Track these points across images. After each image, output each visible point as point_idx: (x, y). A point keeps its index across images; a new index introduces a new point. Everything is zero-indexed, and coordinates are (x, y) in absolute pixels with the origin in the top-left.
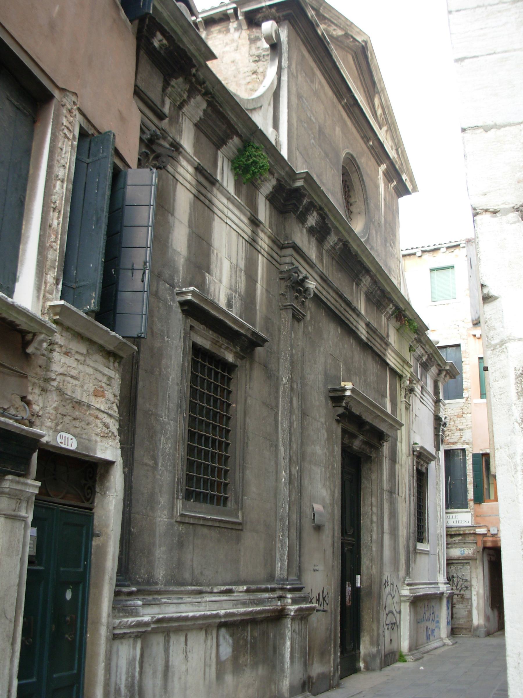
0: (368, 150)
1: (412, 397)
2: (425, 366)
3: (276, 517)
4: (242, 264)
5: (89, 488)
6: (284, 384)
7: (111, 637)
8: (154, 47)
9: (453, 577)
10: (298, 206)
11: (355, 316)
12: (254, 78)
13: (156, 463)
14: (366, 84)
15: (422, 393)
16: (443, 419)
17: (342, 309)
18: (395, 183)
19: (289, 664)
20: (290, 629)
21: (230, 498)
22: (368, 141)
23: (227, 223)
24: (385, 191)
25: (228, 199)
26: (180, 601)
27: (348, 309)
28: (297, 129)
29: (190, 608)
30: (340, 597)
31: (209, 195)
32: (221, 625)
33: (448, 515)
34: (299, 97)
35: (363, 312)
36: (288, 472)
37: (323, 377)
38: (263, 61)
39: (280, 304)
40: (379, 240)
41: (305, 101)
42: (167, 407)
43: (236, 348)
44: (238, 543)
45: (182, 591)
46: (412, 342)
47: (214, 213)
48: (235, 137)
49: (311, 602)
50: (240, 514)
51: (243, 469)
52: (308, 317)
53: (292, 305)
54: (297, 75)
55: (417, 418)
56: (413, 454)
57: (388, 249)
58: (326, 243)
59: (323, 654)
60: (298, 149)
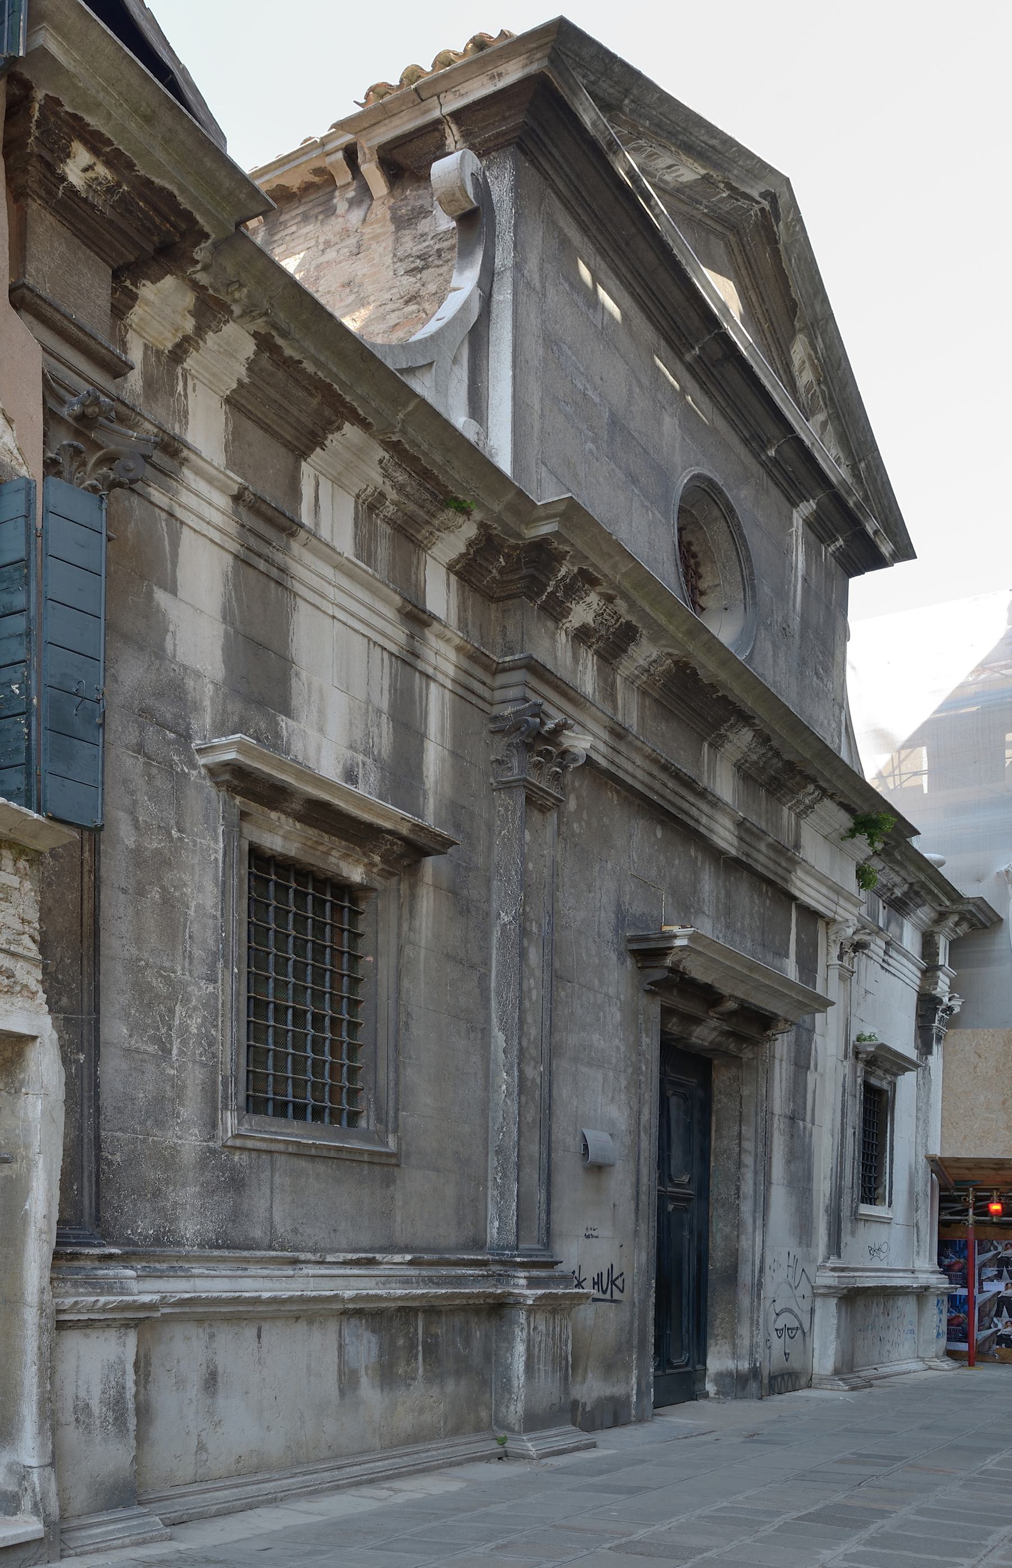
0: (762, 471)
1: (859, 960)
7: (51, 1324)
8: (71, 189)
10: (544, 580)
11: (705, 807)
12: (413, 312)
17: (667, 793)
22: (764, 448)
23: (334, 617)
25: (337, 567)
26: (240, 1273)
27: (684, 792)
28: (542, 416)
29: (258, 1284)
30: (653, 1281)
31: (279, 557)
32: (346, 1314)
34: (551, 341)
36: (516, 1074)
38: (438, 266)
40: (781, 662)
41: (570, 353)
42: (187, 954)
44: (388, 1186)
45: (245, 1257)
47: (296, 594)
49: (579, 1285)
50: (391, 1140)
52: (572, 804)
53: (525, 780)
54: (544, 287)
55: (870, 996)
56: (857, 1058)
60: (544, 463)
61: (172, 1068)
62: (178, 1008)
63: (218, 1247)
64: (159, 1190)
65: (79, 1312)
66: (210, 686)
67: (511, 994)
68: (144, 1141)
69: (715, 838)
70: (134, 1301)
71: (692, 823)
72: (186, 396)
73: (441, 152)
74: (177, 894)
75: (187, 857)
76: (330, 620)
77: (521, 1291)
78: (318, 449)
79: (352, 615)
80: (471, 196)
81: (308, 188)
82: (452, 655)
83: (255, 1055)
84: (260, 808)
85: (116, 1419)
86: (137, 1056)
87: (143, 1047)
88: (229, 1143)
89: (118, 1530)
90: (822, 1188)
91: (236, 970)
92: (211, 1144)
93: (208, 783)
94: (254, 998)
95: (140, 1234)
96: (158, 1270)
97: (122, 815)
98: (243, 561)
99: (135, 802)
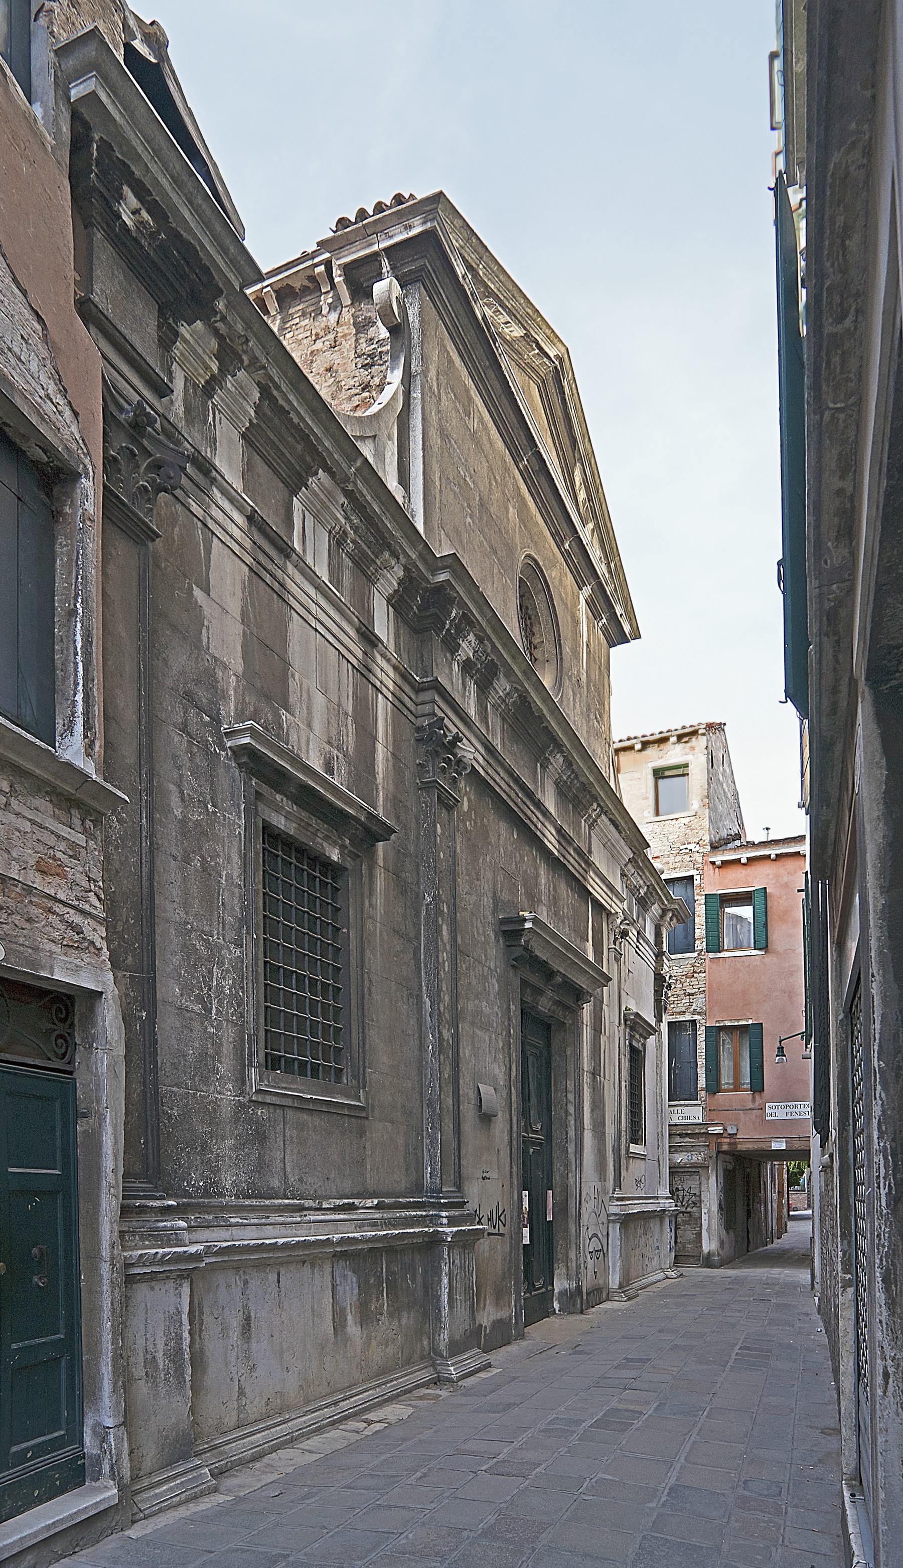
2: (644, 904)
3: (422, 1101)
6: (428, 904)
9: (677, 1189)
12: (366, 398)
14: (560, 444)
15: (638, 941)
16: (667, 978)
23: (316, 630)
25: (317, 588)
28: (441, 491)
33: (672, 1109)
35: (551, 807)
43: (342, 839)
46: (626, 865)
49: (480, 1223)
57: (591, 723)
59: (499, 1295)
63: (249, 1197)
65: (144, 1265)
71: (533, 828)
73: (379, 277)
74: (212, 863)
75: (219, 830)
76: (314, 632)
77: (444, 1229)
81: (305, 290)
85: (176, 1371)
86: (188, 1015)
89: (171, 1489)
90: (610, 1130)
96: (207, 1220)
97: (172, 787)
99: (181, 776)
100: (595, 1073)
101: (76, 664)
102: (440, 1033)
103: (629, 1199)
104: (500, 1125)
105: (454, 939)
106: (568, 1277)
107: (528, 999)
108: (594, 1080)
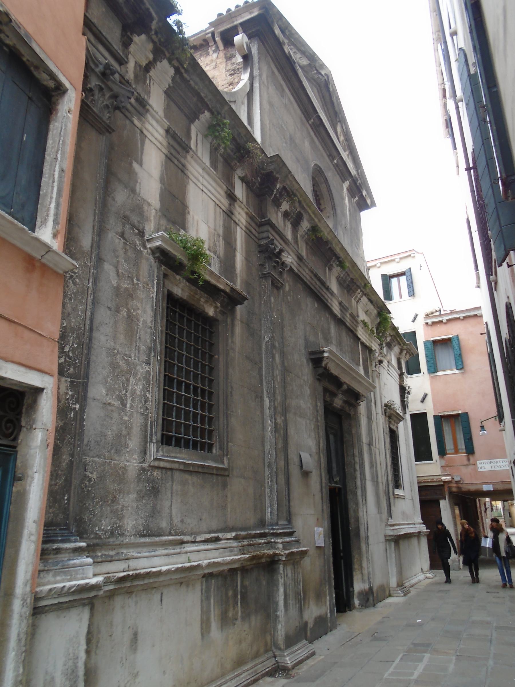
4: (221, 231)
5: (10, 421)
6: (266, 342)
13: (125, 405)
15: (388, 366)
16: (407, 388)
17: (317, 287)
18: (357, 198)
19: (283, 613)
20: (283, 575)
21: (214, 445)
22: (333, 159)
23: (202, 190)
24: (349, 203)
27: (322, 288)
28: (270, 129)
31: (182, 160)
34: (271, 104)
36: (274, 421)
37: (304, 341)
39: (260, 273)
43: (215, 303)
44: (224, 489)
45: (157, 542)
48: (206, 112)
50: (225, 460)
51: (227, 417)
52: (287, 288)
58: (300, 229)
59: (319, 597)
61: (126, 415)
62: (131, 379)
63: (144, 536)
64: (115, 497)
66: (154, 211)
67: (270, 378)
68: (109, 464)
69: (333, 309)
70: (87, 584)
71: (326, 301)
72: (150, 86)
74: (134, 313)
75: (140, 294)
76: (201, 191)
78: (197, 120)
79: (209, 191)
80: (246, 49)
81: (201, 46)
82: (244, 215)
83: (167, 410)
84: (172, 272)
86: (110, 408)
87: (113, 402)
88: (152, 464)
91: (159, 358)
92: (143, 465)
93: (151, 257)
94: (168, 375)
95: (103, 530)
98: (169, 158)
99: (118, 262)
100: (370, 444)
101: (53, 187)
102: (275, 419)
103: (399, 525)
104: (315, 481)
105: (283, 363)
106: (363, 581)
107: (328, 399)
108: (370, 449)
